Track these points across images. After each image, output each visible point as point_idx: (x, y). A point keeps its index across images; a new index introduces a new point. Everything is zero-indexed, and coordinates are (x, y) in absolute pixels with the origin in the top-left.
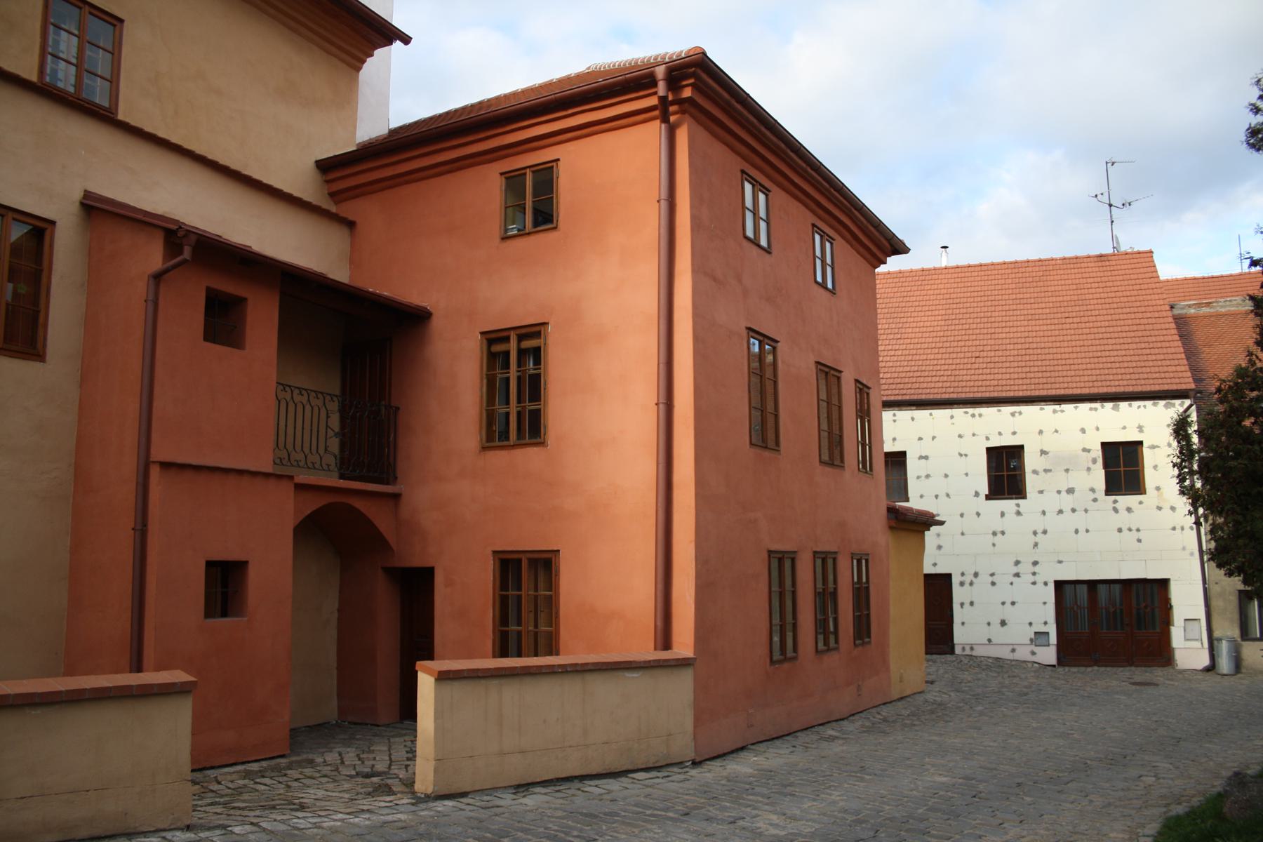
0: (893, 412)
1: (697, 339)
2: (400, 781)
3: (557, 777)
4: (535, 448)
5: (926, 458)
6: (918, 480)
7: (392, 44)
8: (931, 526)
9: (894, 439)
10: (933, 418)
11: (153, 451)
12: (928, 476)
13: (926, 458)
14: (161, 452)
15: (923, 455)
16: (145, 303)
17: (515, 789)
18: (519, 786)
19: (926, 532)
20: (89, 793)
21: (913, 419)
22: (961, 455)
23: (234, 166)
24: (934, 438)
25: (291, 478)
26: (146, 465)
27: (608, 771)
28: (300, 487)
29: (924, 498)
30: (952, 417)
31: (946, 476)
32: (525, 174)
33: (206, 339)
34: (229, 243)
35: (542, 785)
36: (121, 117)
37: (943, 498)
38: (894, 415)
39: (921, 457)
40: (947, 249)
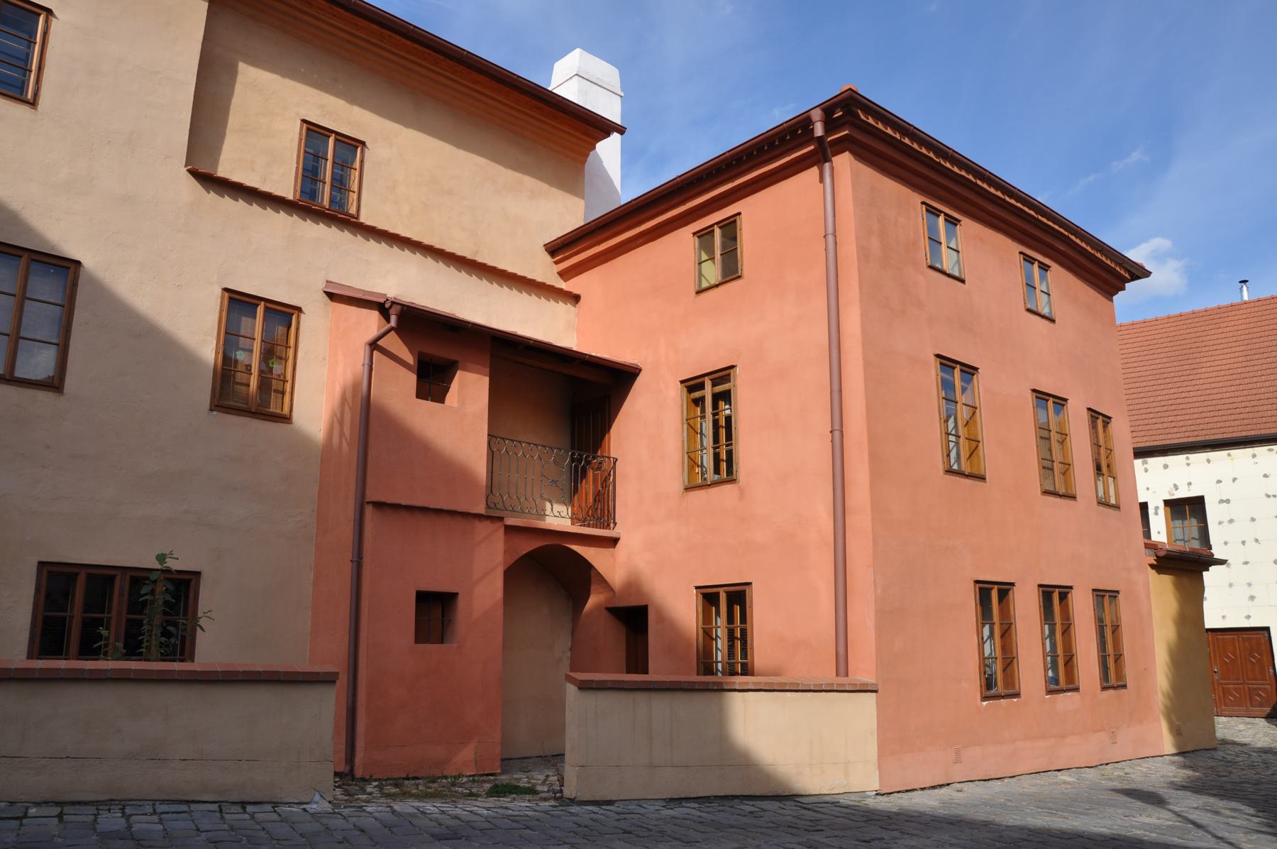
0: (1185, 456)
1: (867, 364)
2: (563, 786)
3: (716, 794)
4: (728, 486)
5: (1228, 501)
6: (1220, 526)
7: (609, 136)
8: (1210, 566)
9: (1190, 484)
10: (1232, 459)
11: (368, 492)
12: (1231, 521)
13: (1228, 501)
14: (372, 495)
15: (1224, 499)
16: (362, 367)
17: (667, 802)
18: (672, 800)
19: (1204, 573)
20: (241, 762)
21: (1209, 461)
22: (1268, 496)
23: (438, 245)
24: (1234, 480)
25: (501, 519)
26: (361, 505)
27: (775, 794)
28: (510, 530)
29: (1228, 544)
30: (1254, 456)
31: (1253, 520)
32: (713, 231)
33: (418, 396)
34: (428, 310)
35: (697, 801)
36: (365, 219)
37: (1250, 543)
38: (1188, 458)
39: (1221, 501)
40: (1247, 283)
